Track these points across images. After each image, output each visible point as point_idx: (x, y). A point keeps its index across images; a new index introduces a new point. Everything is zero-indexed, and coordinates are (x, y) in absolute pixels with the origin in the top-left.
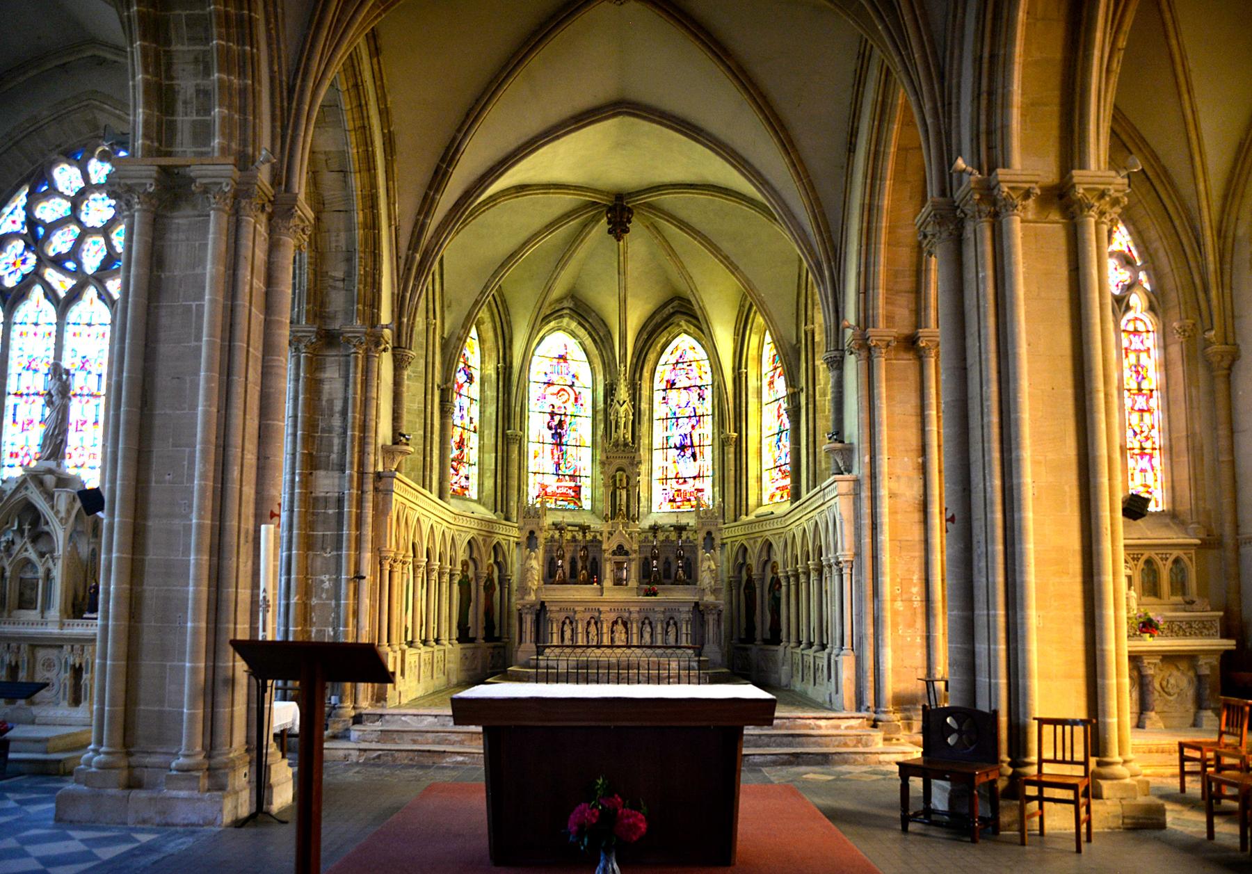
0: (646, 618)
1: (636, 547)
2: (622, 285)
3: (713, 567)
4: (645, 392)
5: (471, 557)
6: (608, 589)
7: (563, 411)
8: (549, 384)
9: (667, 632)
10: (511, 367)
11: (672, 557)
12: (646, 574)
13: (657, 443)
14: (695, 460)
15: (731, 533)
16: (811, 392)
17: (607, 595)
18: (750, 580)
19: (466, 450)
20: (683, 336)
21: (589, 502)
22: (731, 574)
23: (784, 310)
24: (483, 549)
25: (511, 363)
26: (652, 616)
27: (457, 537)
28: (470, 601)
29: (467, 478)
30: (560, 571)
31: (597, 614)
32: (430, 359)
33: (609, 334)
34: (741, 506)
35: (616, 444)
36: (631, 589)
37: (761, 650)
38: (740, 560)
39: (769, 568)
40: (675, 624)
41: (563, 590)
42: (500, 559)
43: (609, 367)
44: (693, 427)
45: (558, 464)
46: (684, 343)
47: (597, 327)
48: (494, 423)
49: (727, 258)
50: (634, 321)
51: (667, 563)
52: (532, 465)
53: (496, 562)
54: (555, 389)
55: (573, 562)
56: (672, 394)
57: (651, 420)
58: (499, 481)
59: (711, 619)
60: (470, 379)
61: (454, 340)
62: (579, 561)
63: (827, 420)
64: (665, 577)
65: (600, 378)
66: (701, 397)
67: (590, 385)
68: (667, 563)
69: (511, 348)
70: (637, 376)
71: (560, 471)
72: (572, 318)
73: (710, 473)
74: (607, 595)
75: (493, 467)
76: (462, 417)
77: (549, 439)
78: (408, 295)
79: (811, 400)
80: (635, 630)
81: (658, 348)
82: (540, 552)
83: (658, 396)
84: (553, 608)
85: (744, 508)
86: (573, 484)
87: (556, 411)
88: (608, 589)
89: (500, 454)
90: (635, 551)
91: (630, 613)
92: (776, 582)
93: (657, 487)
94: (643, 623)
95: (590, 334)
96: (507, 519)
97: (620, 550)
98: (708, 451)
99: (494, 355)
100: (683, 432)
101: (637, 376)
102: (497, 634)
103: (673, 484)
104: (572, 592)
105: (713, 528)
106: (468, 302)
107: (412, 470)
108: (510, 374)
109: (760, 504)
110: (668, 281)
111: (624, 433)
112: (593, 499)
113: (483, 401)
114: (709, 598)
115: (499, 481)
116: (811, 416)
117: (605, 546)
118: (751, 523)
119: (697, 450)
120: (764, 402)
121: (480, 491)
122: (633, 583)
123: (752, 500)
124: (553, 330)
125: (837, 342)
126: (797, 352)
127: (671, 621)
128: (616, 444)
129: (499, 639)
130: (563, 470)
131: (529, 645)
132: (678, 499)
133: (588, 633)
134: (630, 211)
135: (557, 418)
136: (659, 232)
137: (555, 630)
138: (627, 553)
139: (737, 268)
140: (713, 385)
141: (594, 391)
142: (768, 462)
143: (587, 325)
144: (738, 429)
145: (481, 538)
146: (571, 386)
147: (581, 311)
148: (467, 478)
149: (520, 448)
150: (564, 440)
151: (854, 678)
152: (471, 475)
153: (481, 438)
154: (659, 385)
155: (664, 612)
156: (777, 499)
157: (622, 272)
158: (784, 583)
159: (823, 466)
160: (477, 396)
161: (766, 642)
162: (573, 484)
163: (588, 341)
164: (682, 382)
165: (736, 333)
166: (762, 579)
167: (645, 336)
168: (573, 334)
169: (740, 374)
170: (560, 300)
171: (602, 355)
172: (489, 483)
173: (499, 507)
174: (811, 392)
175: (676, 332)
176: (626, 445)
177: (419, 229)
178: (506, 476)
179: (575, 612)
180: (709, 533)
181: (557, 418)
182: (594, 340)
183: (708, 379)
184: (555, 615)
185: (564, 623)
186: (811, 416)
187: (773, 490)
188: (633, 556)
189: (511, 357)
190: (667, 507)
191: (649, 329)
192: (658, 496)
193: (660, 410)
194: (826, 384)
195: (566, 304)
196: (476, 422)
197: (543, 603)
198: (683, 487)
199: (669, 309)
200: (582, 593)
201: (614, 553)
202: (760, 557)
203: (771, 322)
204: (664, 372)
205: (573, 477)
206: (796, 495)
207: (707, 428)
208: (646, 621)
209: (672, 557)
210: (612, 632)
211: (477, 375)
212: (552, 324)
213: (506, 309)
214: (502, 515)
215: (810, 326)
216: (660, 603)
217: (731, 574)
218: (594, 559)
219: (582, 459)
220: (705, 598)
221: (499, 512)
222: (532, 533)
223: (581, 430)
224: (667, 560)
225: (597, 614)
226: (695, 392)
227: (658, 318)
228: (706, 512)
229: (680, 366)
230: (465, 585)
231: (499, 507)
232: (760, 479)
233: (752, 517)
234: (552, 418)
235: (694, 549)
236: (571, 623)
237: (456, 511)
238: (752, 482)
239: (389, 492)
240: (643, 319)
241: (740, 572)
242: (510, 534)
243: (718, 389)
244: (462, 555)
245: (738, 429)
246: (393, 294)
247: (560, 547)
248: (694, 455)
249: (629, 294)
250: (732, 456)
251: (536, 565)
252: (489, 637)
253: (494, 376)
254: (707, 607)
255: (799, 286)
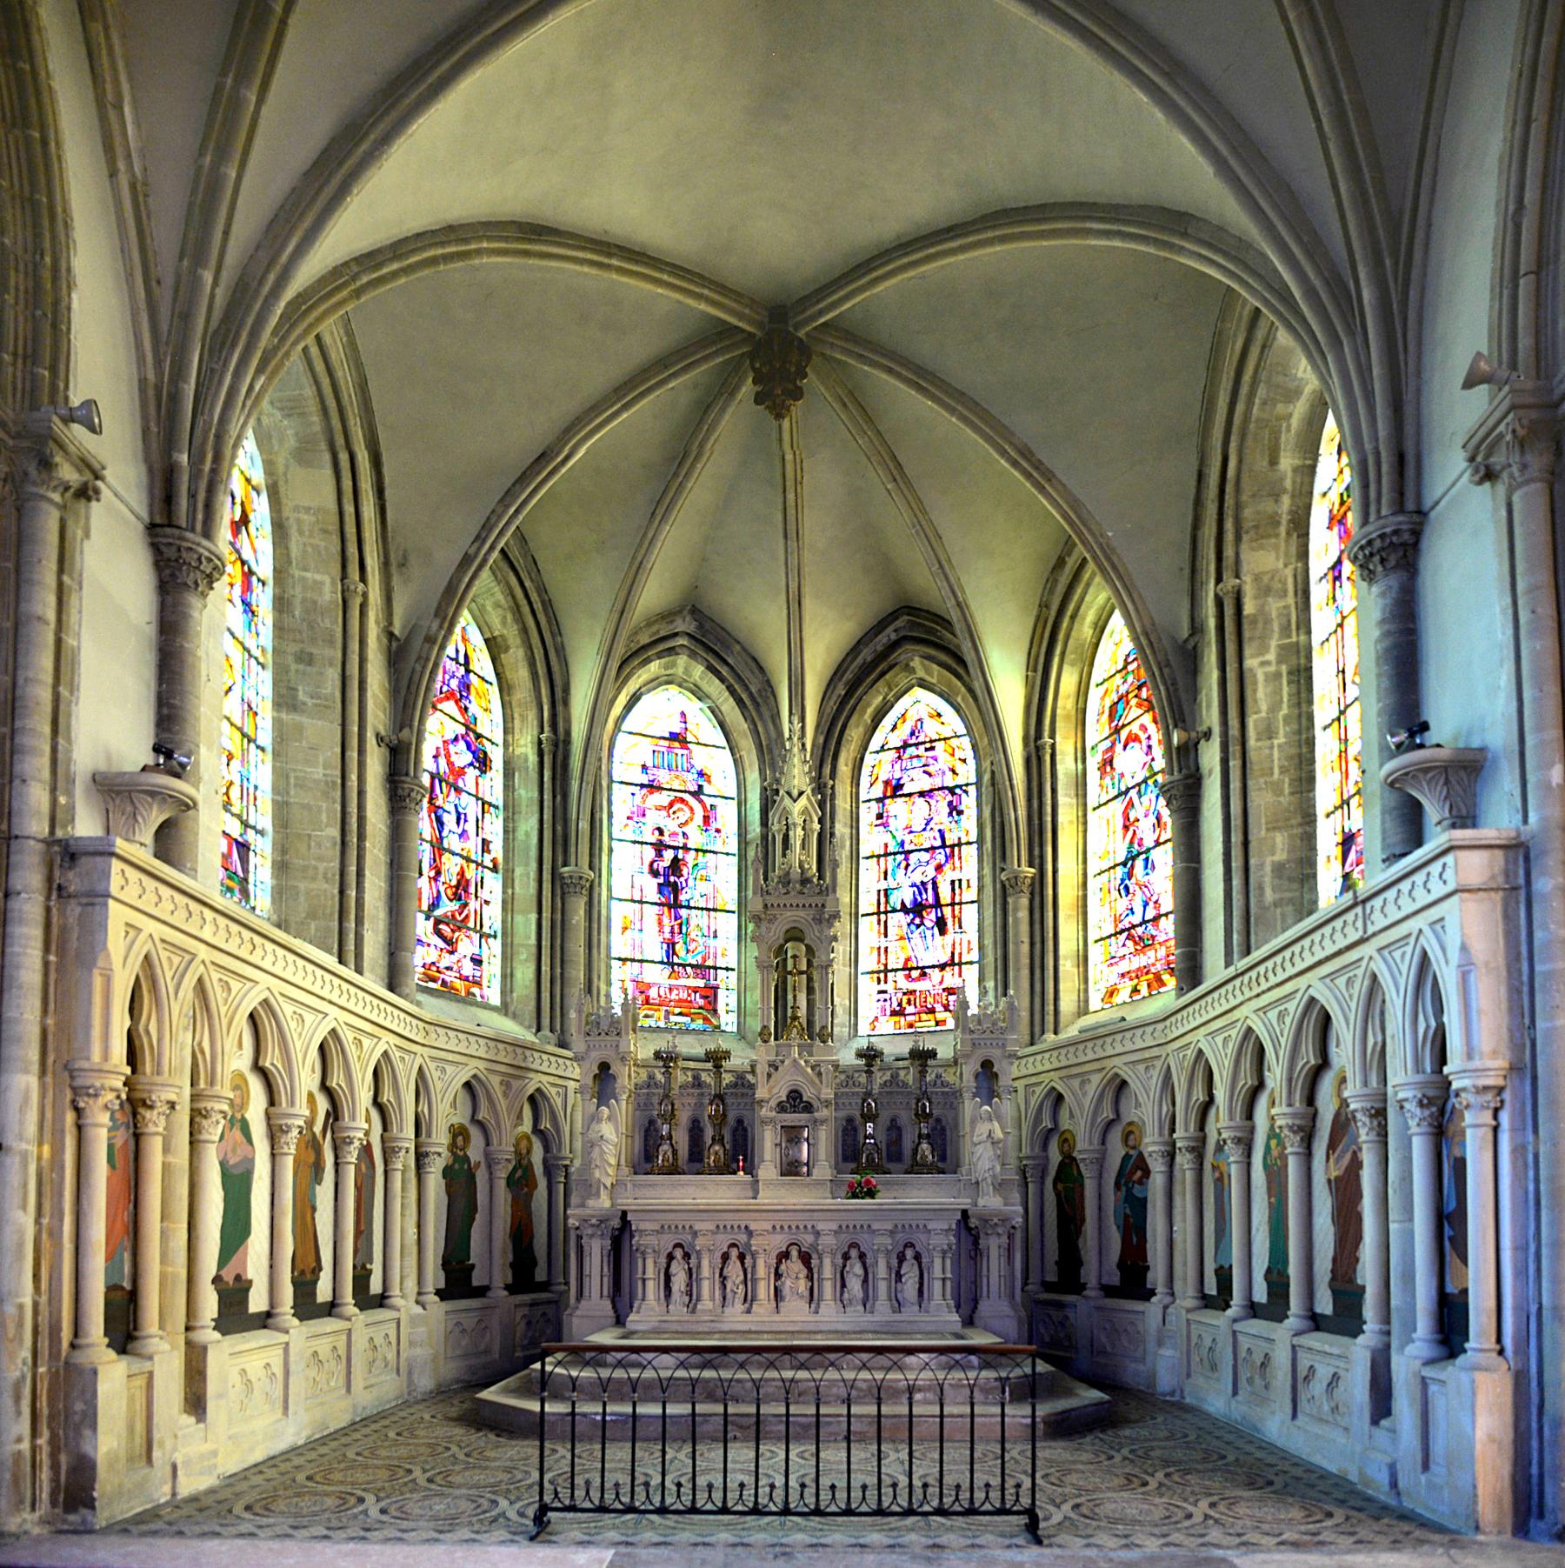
0: (854, 1245)
1: (828, 1093)
2: (793, 561)
3: (999, 1134)
4: (843, 804)
5: (474, 1120)
6: (769, 1183)
7: (680, 842)
8: (652, 787)
9: (899, 1277)
10: (567, 741)
11: (906, 1118)
12: (850, 1151)
13: (867, 903)
14: (943, 932)
15: (1029, 1070)
16: (1234, 731)
17: (766, 1198)
18: (1068, 1162)
19: (473, 905)
20: (918, 692)
21: (733, 1017)
22: (1026, 1151)
23: (1158, 561)
24: (502, 1104)
25: (568, 733)
26: (865, 1241)
27: (433, 1073)
28: (473, 1208)
29: (477, 961)
30: (665, 1147)
31: (743, 1238)
32: (354, 669)
33: (769, 688)
34: (1043, 1013)
35: (786, 880)
36: (819, 1183)
37: (1099, 1308)
38: (1047, 1123)
39: (1116, 1136)
40: (918, 1257)
41: (674, 1186)
42: (545, 1124)
43: (771, 754)
44: (939, 868)
45: (671, 945)
46: (921, 706)
47: (746, 674)
48: (534, 852)
49: (1026, 453)
50: (821, 651)
51: (895, 1127)
52: (620, 944)
53: (536, 1130)
54: (663, 798)
55: (695, 1130)
56: (895, 807)
57: (855, 856)
58: (545, 968)
59: (994, 1246)
60: (482, 762)
61: (417, 643)
62: (706, 1127)
63: (1278, 791)
64: (890, 1159)
65: (753, 777)
66: (955, 810)
67: (734, 794)
68: (895, 1127)
69: (566, 703)
70: (827, 770)
71: (669, 946)
72: (693, 655)
73: (974, 956)
74: (766, 1198)
75: (533, 941)
76: (463, 835)
77: (652, 894)
78: (190, 389)
79: (1234, 749)
80: (828, 1272)
81: (868, 717)
82: (622, 1107)
83: (868, 814)
84: (642, 1226)
85: (1050, 1018)
86: (701, 983)
87: (666, 839)
88: (769, 1183)
89: (546, 914)
90: (827, 1104)
91: (817, 1234)
92: (1135, 1167)
93: (867, 986)
94: (846, 1257)
95: (732, 691)
96: (563, 1044)
97: (795, 1101)
98: (970, 914)
99: (532, 716)
100: (917, 877)
101: (827, 770)
102: (540, 1275)
103: (894, 982)
104: (690, 1190)
105: (995, 1054)
106: (446, 559)
107: (312, 915)
108: (567, 756)
109: (1083, 1010)
110: (883, 566)
111: (801, 857)
112: (741, 1012)
113: (510, 811)
114: (991, 1201)
115: (545, 968)
116: (1235, 785)
117: (761, 1093)
118: (1073, 1043)
119: (947, 911)
120: (1092, 801)
121: (505, 991)
122: (823, 1170)
123: (1068, 1003)
124: (654, 683)
125: (1400, 493)
126: (1191, 659)
127: (907, 1253)
128: (786, 880)
129: (545, 1286)
130: (682, 955)
131: (596, 1302)
132: (910, 1009)
133: (723, 1279)
134: (805, 351)
135: (669, 855)
136: (870, 420)
137: (650, 1273)
138: (808, 1108)
139: (1050, 476)
140: (978, 784)
141: (742, 804)
142: (1101, 922)
143: (724, 671)
144: (1036, 860)
145: (495, 1081)
146: (698, 793)
147: (707, 638)
148: (477, 961)
149: (590, 904)
150: (683, 898)
151: (1508, 1436)
152: (491, 960)
153: (508, 883)
154: (870, 790)
155: (892, 1233)
156: (1123, 995)
157: (791, 533)
158: (1157, 1167)
159: (1269, 896)
160: (497, 797)
161: (1109, 1291)
162: (701, 983)
163: (729, 706)
164: (916, 781)
165: (1031, 666)
166: (1101, 1162)
167: (841, 690)
168: (698, 693)
169: (1039, 749)
170: (667, 616)
171: (755, 732)
172: (525, 974)
173: (546, 1021)
174: (1234, 731)
175: (903, 684)
176: (805, 881)
177: (206, 199)
178: (560, 957)
179: (695, 1234)
180: (987, 1065)
181: (669, 855)
182: (740, 702)
183: (968, 773)
184: (650, 1241)
185: (670, 1257)
186: (1235, 785)
187: (1114, 979)
188: (824, 1113)
189: (568, 721)
190: (887, 1025)
191: (848, 676)
192: (869, 1005)
193: (872, 839)
194: (1275, 708)
195: (681, 625)
196: (497, 850)
197: (624, 1213)
198: (918, 986)
199: (889, 634)
200: (714, 1193)
201: (781, 1108)
202: (1095, 1113)
203: (1128, 596)
204: (879, 766)
205: (701, 969)
206: (1190, 971)
207: (969, 865)
208: (854, 1252)
209: (906, 1118)
210: (778, 1276)
211: (496, 755)
212: (654, 667)
213: (557, 628)
214: (553, 1038)
215: (1230, 582)
216: (881, 1212)
217: (1026, 1151)
218: (740, 1122)
219: (721, 938)
220: (981, 1202)
221: (546, 1032)
222: (604, 1067)
223: (717, 880)
224: (895, 1125)
225: (743, 1238)
226: (942, 800)
227: (866, 654)
228: (979, 1020)
229: (911, 751)
230: (460, 1180)
231: (546, 1021)
232: (1083, 960)
233: (1070, 1032)
234: (659, 854)
235: (953, 1097)
236: (687, 1256)
237: (427, 1016)
238: (1067, 967)
239: (97, 897)
240: (837, 656)
241: (1045, 1146)
242: (562, 1075)
243: (993, 787)
244: (447, 1112)
245: (1036, 860)
246: (143, 382)
247: (667, 1096)
248: (941, 924)
249: (806, 590)
250: (1023, 914)
251: (612, 1134)
252: (523, 1276)
253: (533, 758)
254: (985, 1221)
255: (1198, 503)
